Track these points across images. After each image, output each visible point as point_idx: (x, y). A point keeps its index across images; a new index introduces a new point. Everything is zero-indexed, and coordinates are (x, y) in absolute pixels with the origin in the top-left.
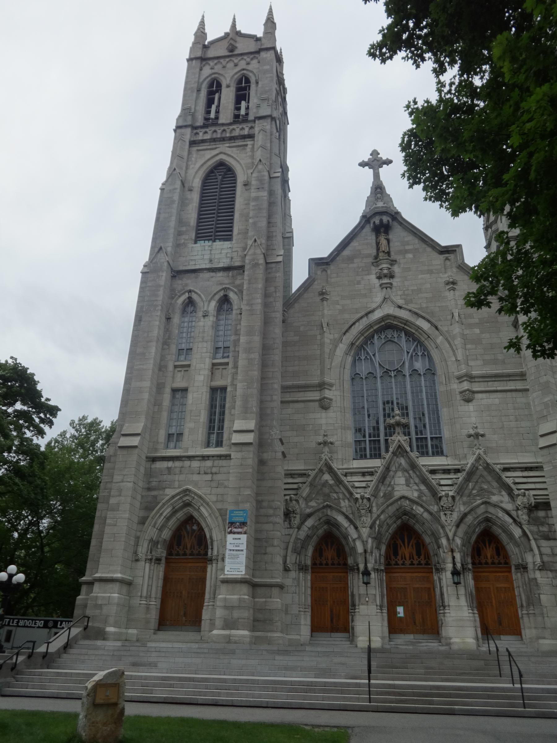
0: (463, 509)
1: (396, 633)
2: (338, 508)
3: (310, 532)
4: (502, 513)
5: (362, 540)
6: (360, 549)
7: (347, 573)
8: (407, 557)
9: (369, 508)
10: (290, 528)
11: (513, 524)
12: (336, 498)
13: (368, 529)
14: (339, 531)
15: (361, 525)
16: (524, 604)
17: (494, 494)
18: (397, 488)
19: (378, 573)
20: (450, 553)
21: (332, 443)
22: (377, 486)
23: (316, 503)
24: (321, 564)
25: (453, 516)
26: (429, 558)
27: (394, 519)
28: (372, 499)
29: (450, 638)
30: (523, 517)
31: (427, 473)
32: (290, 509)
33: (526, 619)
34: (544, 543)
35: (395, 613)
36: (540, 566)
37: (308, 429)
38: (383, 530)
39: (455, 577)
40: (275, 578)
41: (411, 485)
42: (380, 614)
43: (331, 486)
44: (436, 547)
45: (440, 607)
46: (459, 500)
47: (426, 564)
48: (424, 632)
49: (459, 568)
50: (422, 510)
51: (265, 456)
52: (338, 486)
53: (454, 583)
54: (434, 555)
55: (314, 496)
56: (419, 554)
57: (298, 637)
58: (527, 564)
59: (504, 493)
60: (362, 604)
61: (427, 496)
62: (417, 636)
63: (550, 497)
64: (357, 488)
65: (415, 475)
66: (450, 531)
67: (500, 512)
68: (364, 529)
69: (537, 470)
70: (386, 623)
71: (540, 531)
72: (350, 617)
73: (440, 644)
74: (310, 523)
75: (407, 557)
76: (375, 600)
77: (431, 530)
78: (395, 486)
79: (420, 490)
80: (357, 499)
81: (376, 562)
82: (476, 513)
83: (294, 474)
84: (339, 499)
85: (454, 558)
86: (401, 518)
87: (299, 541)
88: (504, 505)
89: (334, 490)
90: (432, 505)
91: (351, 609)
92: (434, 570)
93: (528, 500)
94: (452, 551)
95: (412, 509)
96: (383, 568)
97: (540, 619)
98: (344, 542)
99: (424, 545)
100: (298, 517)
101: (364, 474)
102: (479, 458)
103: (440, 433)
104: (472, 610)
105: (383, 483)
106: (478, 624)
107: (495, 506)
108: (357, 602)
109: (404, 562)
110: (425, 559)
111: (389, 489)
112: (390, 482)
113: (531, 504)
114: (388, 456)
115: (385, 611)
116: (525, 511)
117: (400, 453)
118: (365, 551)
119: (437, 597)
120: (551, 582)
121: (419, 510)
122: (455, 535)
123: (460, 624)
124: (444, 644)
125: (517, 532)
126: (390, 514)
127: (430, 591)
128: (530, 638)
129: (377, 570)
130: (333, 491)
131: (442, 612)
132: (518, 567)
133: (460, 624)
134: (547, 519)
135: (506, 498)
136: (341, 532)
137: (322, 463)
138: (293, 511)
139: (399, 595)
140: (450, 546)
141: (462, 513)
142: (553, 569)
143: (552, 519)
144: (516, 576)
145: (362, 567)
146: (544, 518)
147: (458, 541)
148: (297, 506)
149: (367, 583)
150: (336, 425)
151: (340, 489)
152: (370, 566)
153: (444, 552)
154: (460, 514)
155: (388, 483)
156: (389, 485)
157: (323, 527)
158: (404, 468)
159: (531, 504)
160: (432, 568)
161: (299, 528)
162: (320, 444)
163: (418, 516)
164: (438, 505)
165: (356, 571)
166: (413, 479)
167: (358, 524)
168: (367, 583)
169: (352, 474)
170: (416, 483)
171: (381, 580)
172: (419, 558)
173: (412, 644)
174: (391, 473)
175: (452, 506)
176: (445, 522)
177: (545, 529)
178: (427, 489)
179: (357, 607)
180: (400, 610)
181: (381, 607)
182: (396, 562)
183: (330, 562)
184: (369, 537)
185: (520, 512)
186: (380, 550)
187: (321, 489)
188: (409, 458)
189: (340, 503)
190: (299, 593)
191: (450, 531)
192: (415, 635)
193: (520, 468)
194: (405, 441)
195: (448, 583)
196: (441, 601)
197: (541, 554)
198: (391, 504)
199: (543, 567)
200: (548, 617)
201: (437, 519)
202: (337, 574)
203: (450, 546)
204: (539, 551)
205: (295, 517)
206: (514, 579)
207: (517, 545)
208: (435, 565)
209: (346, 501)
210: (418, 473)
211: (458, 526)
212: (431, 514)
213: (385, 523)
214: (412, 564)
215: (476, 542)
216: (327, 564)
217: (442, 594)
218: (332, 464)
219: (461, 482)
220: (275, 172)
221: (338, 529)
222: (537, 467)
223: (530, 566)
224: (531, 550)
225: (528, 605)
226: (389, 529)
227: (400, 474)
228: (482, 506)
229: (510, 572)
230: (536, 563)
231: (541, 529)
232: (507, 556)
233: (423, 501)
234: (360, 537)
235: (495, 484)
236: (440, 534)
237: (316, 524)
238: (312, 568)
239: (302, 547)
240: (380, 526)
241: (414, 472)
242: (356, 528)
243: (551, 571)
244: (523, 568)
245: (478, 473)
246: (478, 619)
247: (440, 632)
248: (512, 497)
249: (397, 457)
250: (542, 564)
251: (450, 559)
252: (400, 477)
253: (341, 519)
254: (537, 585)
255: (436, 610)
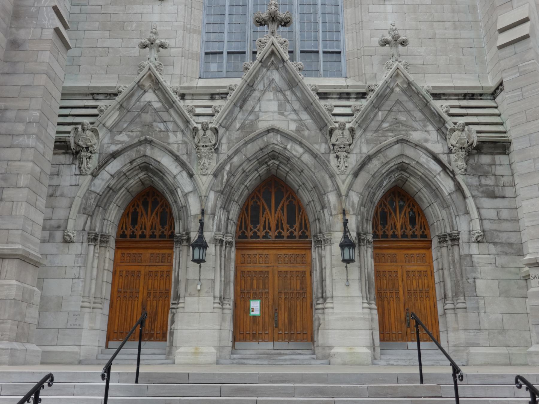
0: (366, 150)
1: (246, 341)
2: (165, 144)
3: (113, 182)
4: (425, 157)
5: (200, 196)
6: (194, 208)
7: (173, 249)
8: (273, 226)
9: (215, 145)
10: (80, 175)
11: (442, 174)
12: (163, 129)
13: (211, 177)
14: (164, 183)
15: (200, 172)
16: (450, 294)
17: (416, 130)
18: (263, 116)
19: (221, 246)
20: (340, 216)
21: (162, 46)
22: (231, 112)
23: (129, 136)
24: (133, 236)
25: (349, 160)
26: (306, 228)
27: (255, 163)
28: (221, 131)
29: (331, 348)
30: (457, 162)
31: (314, 94)
32: (81, 143)
33: (450, 316)
34: (486, 202)
35: (248, 309)
36: (478, 237)
37: (129, 28)
38: (235, 181)
39: (346, 251)
40: (13, 243)
41: (286, 113)
42: (219, 311)
43: (156, 111)
44: (319, 208)
45: (318, 299)
46: (361, 136)
47: (300, 237)
48: (290, 337)
49: (354, 238)
50: (301, 150)
51: (22, 34)
52: (168, 111)
53: (344, 261)
54: (315, 220)
55: (125, 126)
56: (291, 222)
57: (76, 349)
58: (458, 234)
59: (430, 128)
60: (190, 295)
61: (311, 130)
62: (278, 345)
63: (508, 126)
64: (198, 115)
65: (294, 98)
66: (343, 183)
67: (424, 155)
68: (204, 178)
69: (481, 99)
70: (228, 325)
71: (481, 185)
72: (170, 316)
73: (314, 356)
74: (114, 166)
75: (273, 226)
76: (213, 288)
77: (313, 181)
78: (261, 114)
79: (301, 120)
80: (195, 130)
81: (219, 229)
82: (385, 157)
83: (98, 94)
84: (167, 131)
85: (346, 222)
86: (266, 163)
87: (93, 196)
88: (429, 146)
89: (160, 117)
90: (317, 143)
91: (173, 304)
92: (313, 244)
93: (469, 137)
94: (344, 212)
95: (285, 149)
96: (230, 239)
97: (473, 316)
98: (170, 200)
99: (300, 209)
100: (95, 157)
101: (212, 96)
102: (396, 75)
103: (338, 47)
104: (369, 303)
105: (241, 107)
106: (376, 325)
107: (416, 146)
108: (182, 293)
109: (267, 233)
110: (300, 228)
111: (252, 117)
112: (254, 108)
113: (472, 144)
114: (253, 65)
115: (229, 306)
116: (463, 153)
117: (272, 63)
118: (203, 212)
119: (315, 284)
120: (494, 260)
121: (295, 150)
122: (350, 188)
123: (347, 317)
124: (320, 356)
125: (446, 185)
126: (248, 156)
127: (304, 277)
128: (455, 346)
129: (221, 241)
130: (158, 119)
131: (320, 306)
132: (443, 239)
133: (347, 317)
134: (493, 167)
135: (434, 135)
136: (165, 184)
137: (142, 73)
138: (87, 148)
139: (255, 282)
140: (341, 201)
141: (364, 156)
142: (497, 240)
143: (501, 167)
144: (439, 254)
145: (194, 236)
146: (490, 165)
147: (355, 198)
148: (94, 141)
149: (199, 261)
150: (175, 24)
151: (171, 116)
152: (208, 236)
153: (331, 215)
154: (361, 157)
155: (250, 109)
156: (252, 112)
157: (137, 175)
158: (277, 86)
159: (472, 144)
160: (310, 242)
161: (94, 175)
162: (144, 46)
163: (294, 160)
164: (326, 143)
165: (185, 243)
166: (291, 104)
167: (195, 170)
168: (199, 261)
169: (193, 96)
170: (294, 110)
171: (227, 259)
172: (291, 227)
173: (269, 356)
174: (256, 94)
175: (350, 145)
176: (336, 170)
177: (489, 181)
178: (312, 119)
179: (181, 300)
180: (255, 306)
181: (222, 300)
182: (255, 233)
183: (148, 233)
184: (211, 189)
185: (452, 156)
186: (228, 212)
187: (139, 115)
188: (287, 71)
189: (168, 136)
190: (85, 279)
191: (343, 183)
192: (276, 343)
193: (456, 95)
194: (281, 44)
195: (334, 262)
196: (320, 291)
197: (481, 219)
198: (252, 140)
199: (482, 239)
200: (485, 312)
201: (325, 165)
202: (157, 251)
203: (341, 201)
204: (479, 213)
205: (90, 158)
206: (434, 258)
207: (445, 205)
208: (315, 236)
209: (179, 134)
210: (299, 94)
211: (356, 175)
212: (315, 156)
213: (240, 169)
214: (280, 236)
215: (382, 203)
216: (143, 236)
217: (322, 280)
218: (159, 76)
219: (366, 109)
220: (317, 304)
221: (162, 179)
222: (481, 95)
223: (464, 237)
224: (467, 213)
225: (456, 295)
226: (245, 180)
227: (270, 95)
228: (396, 146)
229: (429, 248)
230: (472, 233)
231: (483, 181)
232: (425, 226)
233: (303, 136)
234: (195, 190)
235: (418, 115)
236: (327, 186)
237: (125, 169)
238: (117, 241)
239: (97, 205)
240: (231, 174)
241: (293, 93)
242: (191, 176)
243: (495, 244)
244: (451, 240)
245: (393, 98)
246: (376, 317)
247: (315, 339)
248: (443, 133)
249: (268, 70)
250: (482, 233)
251: (339, 226)
252: (270, 100)
253: (167, 163)
254: (472, 265)
255: (311, 304)
